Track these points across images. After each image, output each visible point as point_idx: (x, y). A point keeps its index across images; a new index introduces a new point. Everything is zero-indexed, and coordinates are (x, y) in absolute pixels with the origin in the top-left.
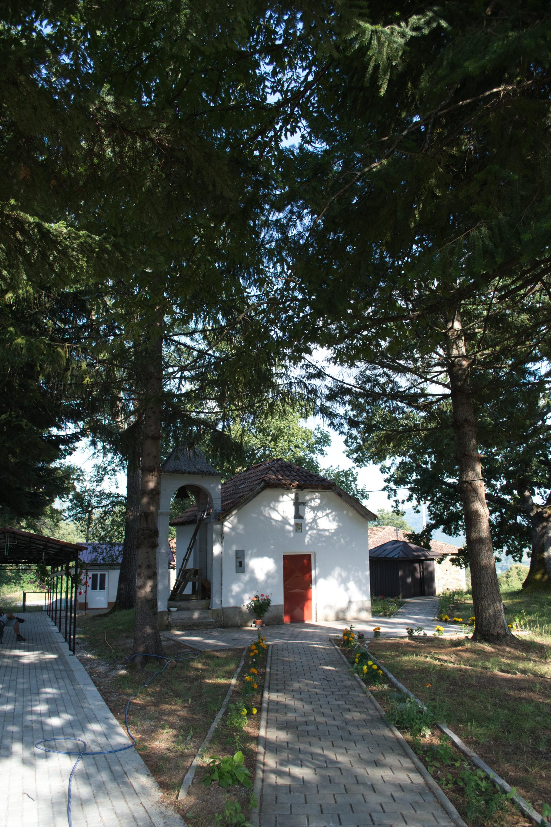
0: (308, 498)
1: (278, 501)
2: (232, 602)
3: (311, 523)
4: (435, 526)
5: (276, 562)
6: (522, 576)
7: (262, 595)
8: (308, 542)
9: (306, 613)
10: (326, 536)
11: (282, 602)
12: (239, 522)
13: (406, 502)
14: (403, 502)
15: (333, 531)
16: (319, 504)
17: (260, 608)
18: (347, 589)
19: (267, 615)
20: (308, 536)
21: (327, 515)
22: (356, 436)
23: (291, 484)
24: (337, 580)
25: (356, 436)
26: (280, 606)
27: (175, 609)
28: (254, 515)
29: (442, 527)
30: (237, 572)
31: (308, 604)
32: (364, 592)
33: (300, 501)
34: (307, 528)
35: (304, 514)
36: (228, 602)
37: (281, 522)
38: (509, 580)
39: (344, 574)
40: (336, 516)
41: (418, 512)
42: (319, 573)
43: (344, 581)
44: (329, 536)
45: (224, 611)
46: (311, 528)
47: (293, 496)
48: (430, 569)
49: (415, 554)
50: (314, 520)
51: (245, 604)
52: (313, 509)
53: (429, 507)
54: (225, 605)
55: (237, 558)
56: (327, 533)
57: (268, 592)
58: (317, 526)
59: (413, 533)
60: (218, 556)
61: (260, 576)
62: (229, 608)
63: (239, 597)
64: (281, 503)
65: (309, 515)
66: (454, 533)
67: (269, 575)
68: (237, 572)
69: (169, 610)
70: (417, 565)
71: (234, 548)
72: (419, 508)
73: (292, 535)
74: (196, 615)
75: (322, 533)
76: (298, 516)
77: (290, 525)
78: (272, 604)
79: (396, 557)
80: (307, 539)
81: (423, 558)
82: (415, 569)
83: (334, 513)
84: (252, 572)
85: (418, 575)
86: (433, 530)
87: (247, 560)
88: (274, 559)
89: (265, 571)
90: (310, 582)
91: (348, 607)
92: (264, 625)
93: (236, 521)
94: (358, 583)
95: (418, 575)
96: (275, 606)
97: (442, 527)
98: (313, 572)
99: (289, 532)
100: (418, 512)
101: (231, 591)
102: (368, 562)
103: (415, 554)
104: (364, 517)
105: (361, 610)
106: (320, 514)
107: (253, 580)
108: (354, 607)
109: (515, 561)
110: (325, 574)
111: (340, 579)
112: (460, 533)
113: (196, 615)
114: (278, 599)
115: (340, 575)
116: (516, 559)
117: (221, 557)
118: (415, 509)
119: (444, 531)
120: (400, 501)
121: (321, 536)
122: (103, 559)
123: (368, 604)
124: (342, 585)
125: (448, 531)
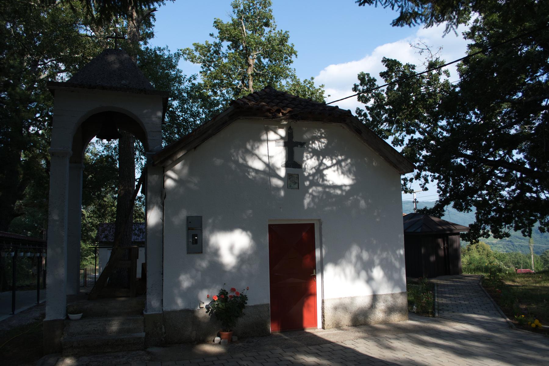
0: (306, 136)
1: (260, 141)
2: (180, 304)
3: (314, 175)
4: (446, 202)
5: (255, 238)
6: (479, 249)
7: (233, 290)
8: (309, 204)
9: (306, 315)
10: (337, 196)
11: (267, 300)
12: (192, 172)
13: (414, 180)
14: (411, 180)
15: (348, 188)
16: (326, 146)
17: (230, 309)
18: (370, 280)
19: (241, 321)
20: (308, 195)
21: (339, 163)
22: (365, 113)
23: (279, 111)
24: (355, 266)
25: (365, 113)
26: (262, 306)
27: (79, 316)
28: (218, 162)
29: (452, 203)
30: (189, 252)
31: (310, 301)
32: (396, 283)
33: (295, 140)
34: (307, 183)
35: (303, 161)
36: (176, 304)
37: (264, 172)
38: (470, 251)
39: (365, 256)
40: (352, 165)
41: (426, 189)
42: (327, 254)
43: (366, 267)
44: (341, 195)
45: (165, 317)
46: (314, 183)
47: (282, 132)
48: (455, 245)
49: (440, 228)
50: (319, 171)
51: (204, 306)
52: (316, 153)
53: (438, 184)
54: (167, 308)
55: (189, 229)
56: (339, 192)
57: (241, 287)
58: (324, 180)
59: (425, 209)
60: (157, 225)
61: (228, 259)
62: (175, 312)
63: (191, 295)
64: (265, 144)
65: (310, 163)
66: (465, 209)
67: (242, 258)
68: (189, 252)
69: (68, 318)
70: (440, 241)
71: (184, 214)
72: (427, 185)
73: (282, 193)
74: (114, 326)
75: (332, 191)
76: (293, 163)
77: (279, 177)
78: (250, 303)
79: (419, 230)
80: (307, 200)
81: (448, 232)
82: (438, 246)
83: (349, 161)
84: (216, 252)
85: (441, 253)
86: (446, 206)
87: (206, 233)
88: (252, 232)
89: (237, 251)
90: (314, 267)
91: (373, 306)
92: (235, 338)
93: (185, 171)
94: (388, 268)
95: (441, 253)
96: (255, 307)
97: (452, 203)
98: (318, 254)
99: (277, 188)
100: (426, 189)
101: (178, 284)
102: (402, 236)
103: (440, 228)
104: (395, 166)
105: (390, 310)
106: (327, 162)
107: (217, 266)
108: (381, 306)
109: (525, 236)
110: (336, 258)
111: (359, 265)
112: (471, 208)
113: (114, 326)
114: (259, 295)
115: (359, 258)
116: (526, 234)
117: (161, 227)
118: (423, 187)
119: (454, 207)
120: (408, 179)
121: (329, 195)
122: (106, 237)
123: (402, 301)
124: (363, 274)
125: (459, 207)
